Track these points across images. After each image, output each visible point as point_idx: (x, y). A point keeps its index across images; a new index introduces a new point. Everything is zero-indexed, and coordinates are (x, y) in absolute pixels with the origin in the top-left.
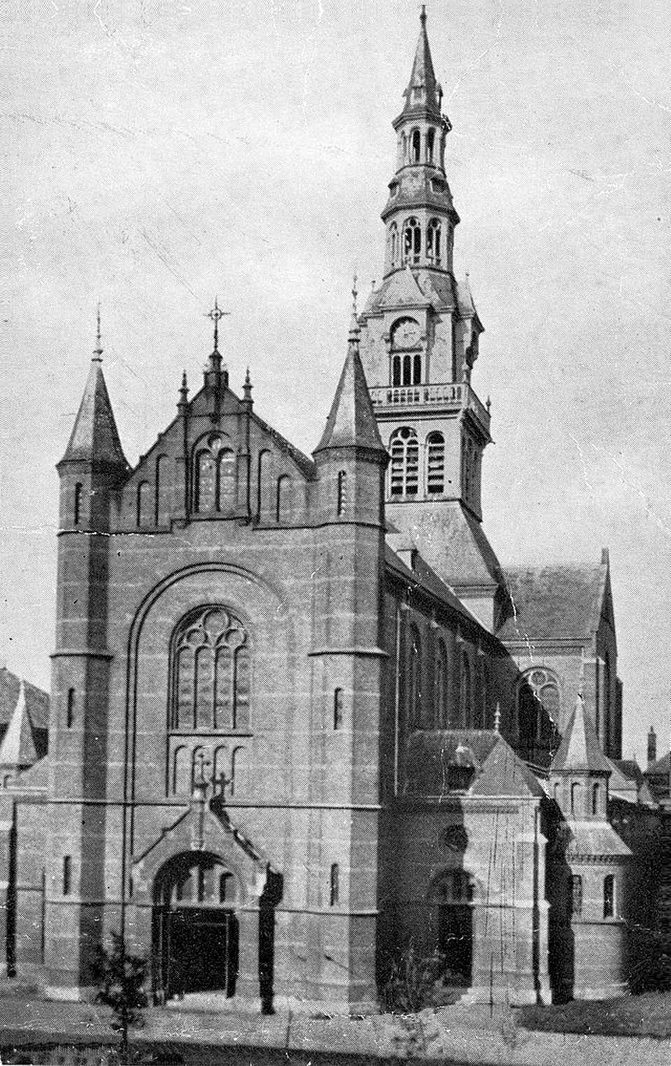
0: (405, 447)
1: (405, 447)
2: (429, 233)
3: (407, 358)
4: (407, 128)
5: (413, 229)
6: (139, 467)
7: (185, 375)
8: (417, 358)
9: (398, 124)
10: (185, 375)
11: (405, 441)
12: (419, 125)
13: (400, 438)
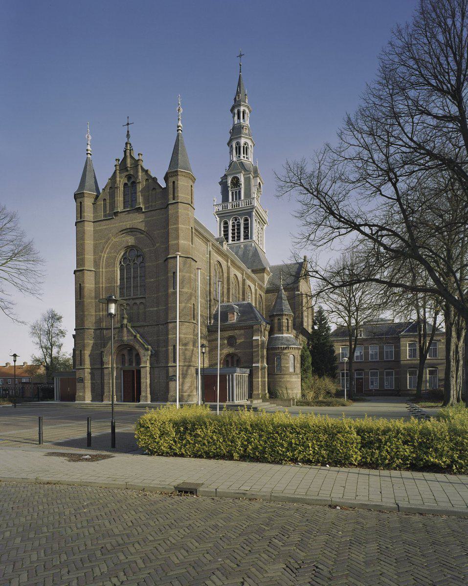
2: (244, 147)
7: (128, 132)
10: (128, 132)
11: (236, 222)
13: (234, 221)
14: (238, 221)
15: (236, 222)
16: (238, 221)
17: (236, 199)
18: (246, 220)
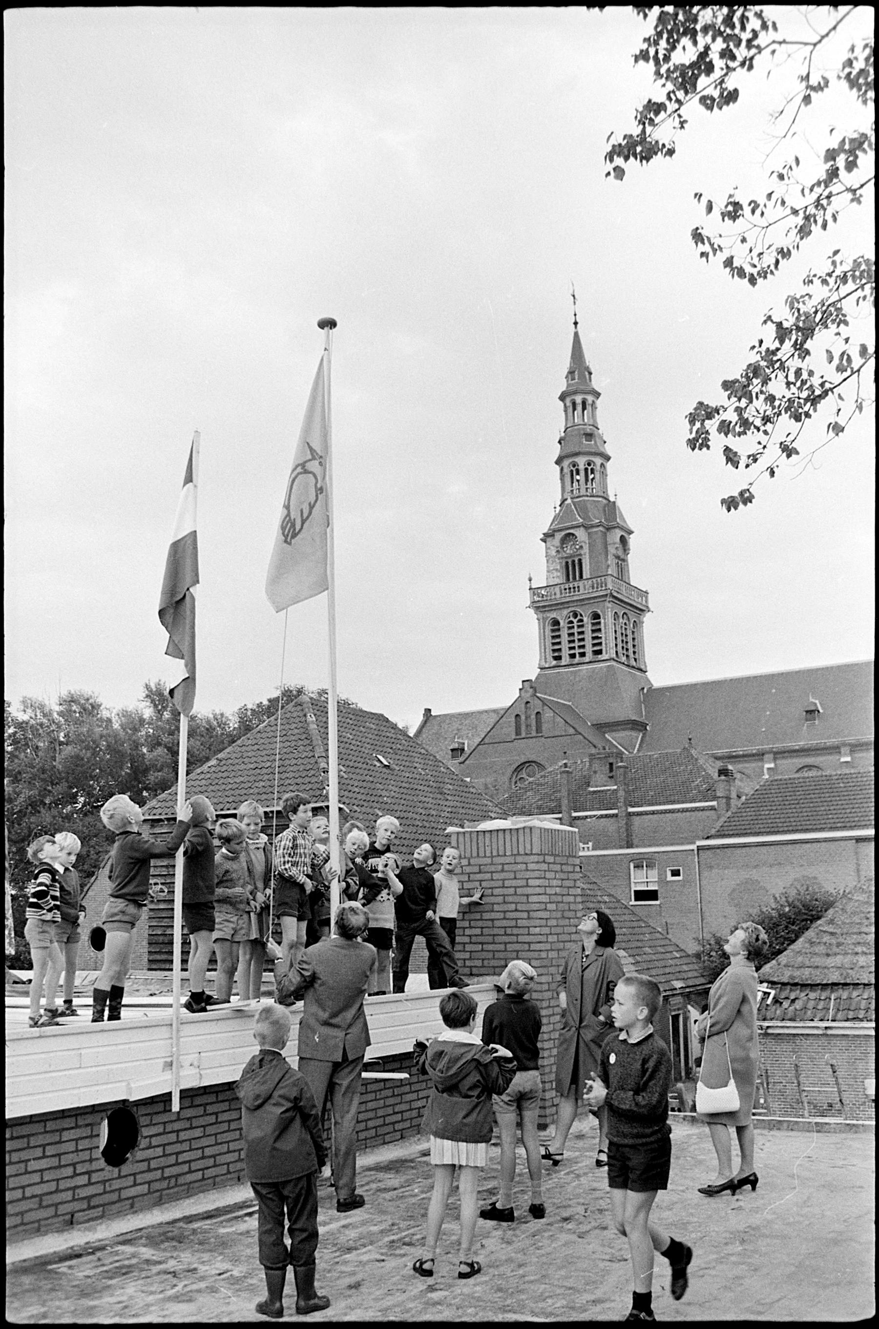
0: (575, 624)
1: (575, 624)
3: (573, 561)
4: (568, 401)
5: (574, 469)
6: (419, 732)
8: (580, 560)
9: (562, 398)
11: (575, 621)
12: (576, 460)
13: (572, 619)
14: (579, 617)
15: (575, 621)
16: (579, 617)
17: (574, 578)
18: (596, 616)
